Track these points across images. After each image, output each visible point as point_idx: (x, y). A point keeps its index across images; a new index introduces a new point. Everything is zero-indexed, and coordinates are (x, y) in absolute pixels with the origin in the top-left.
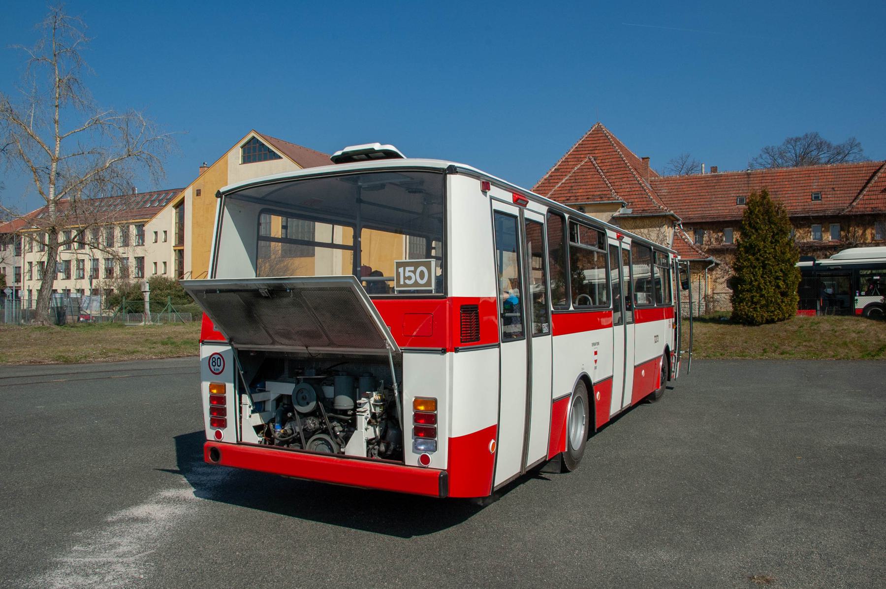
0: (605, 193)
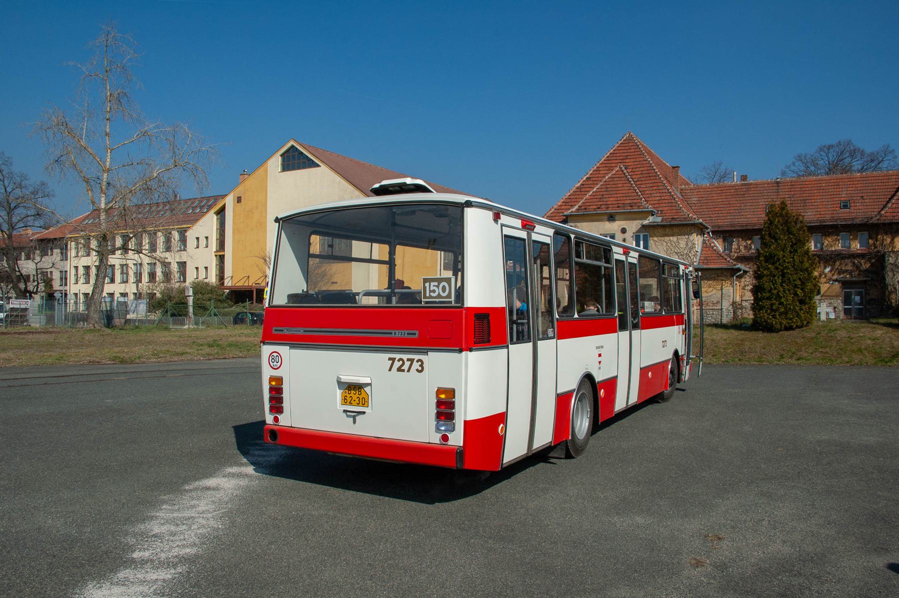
0: (635, 201)
